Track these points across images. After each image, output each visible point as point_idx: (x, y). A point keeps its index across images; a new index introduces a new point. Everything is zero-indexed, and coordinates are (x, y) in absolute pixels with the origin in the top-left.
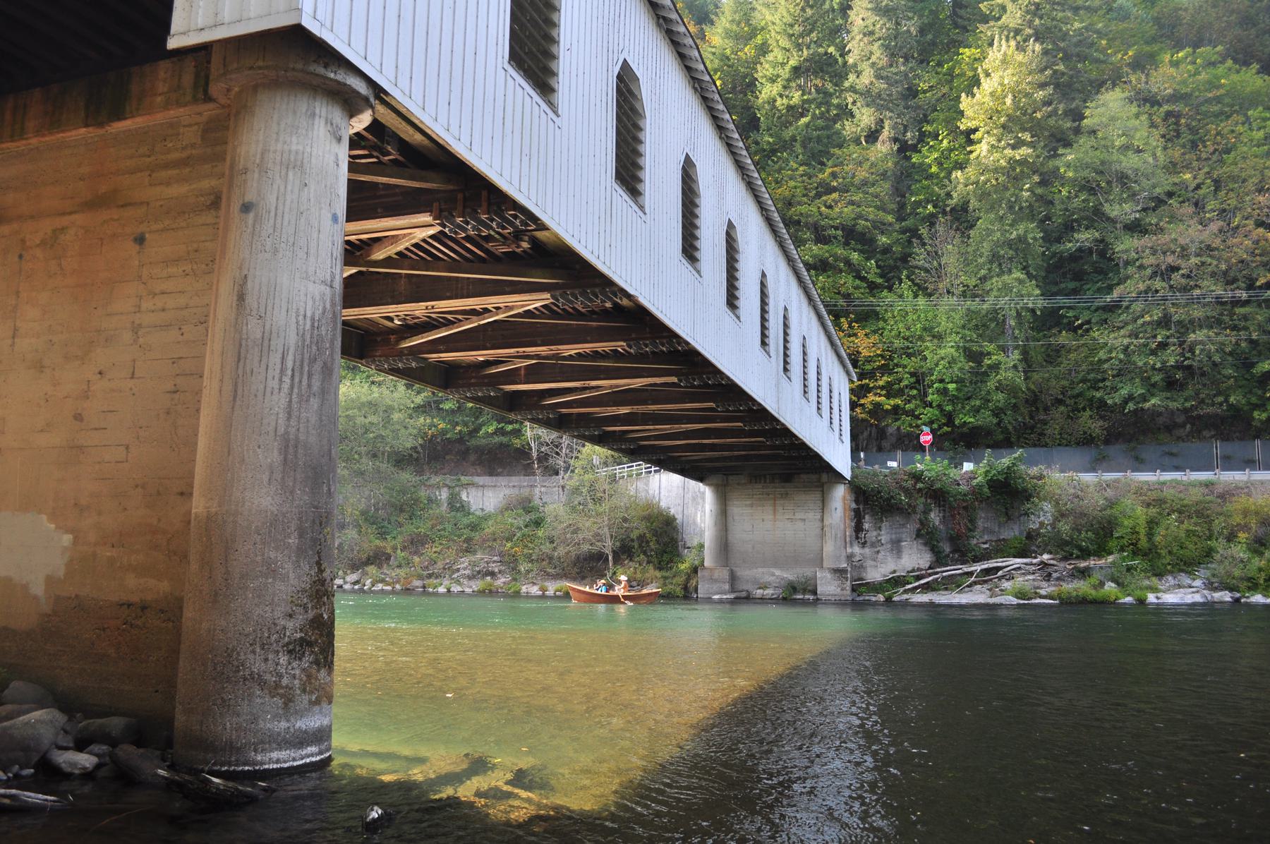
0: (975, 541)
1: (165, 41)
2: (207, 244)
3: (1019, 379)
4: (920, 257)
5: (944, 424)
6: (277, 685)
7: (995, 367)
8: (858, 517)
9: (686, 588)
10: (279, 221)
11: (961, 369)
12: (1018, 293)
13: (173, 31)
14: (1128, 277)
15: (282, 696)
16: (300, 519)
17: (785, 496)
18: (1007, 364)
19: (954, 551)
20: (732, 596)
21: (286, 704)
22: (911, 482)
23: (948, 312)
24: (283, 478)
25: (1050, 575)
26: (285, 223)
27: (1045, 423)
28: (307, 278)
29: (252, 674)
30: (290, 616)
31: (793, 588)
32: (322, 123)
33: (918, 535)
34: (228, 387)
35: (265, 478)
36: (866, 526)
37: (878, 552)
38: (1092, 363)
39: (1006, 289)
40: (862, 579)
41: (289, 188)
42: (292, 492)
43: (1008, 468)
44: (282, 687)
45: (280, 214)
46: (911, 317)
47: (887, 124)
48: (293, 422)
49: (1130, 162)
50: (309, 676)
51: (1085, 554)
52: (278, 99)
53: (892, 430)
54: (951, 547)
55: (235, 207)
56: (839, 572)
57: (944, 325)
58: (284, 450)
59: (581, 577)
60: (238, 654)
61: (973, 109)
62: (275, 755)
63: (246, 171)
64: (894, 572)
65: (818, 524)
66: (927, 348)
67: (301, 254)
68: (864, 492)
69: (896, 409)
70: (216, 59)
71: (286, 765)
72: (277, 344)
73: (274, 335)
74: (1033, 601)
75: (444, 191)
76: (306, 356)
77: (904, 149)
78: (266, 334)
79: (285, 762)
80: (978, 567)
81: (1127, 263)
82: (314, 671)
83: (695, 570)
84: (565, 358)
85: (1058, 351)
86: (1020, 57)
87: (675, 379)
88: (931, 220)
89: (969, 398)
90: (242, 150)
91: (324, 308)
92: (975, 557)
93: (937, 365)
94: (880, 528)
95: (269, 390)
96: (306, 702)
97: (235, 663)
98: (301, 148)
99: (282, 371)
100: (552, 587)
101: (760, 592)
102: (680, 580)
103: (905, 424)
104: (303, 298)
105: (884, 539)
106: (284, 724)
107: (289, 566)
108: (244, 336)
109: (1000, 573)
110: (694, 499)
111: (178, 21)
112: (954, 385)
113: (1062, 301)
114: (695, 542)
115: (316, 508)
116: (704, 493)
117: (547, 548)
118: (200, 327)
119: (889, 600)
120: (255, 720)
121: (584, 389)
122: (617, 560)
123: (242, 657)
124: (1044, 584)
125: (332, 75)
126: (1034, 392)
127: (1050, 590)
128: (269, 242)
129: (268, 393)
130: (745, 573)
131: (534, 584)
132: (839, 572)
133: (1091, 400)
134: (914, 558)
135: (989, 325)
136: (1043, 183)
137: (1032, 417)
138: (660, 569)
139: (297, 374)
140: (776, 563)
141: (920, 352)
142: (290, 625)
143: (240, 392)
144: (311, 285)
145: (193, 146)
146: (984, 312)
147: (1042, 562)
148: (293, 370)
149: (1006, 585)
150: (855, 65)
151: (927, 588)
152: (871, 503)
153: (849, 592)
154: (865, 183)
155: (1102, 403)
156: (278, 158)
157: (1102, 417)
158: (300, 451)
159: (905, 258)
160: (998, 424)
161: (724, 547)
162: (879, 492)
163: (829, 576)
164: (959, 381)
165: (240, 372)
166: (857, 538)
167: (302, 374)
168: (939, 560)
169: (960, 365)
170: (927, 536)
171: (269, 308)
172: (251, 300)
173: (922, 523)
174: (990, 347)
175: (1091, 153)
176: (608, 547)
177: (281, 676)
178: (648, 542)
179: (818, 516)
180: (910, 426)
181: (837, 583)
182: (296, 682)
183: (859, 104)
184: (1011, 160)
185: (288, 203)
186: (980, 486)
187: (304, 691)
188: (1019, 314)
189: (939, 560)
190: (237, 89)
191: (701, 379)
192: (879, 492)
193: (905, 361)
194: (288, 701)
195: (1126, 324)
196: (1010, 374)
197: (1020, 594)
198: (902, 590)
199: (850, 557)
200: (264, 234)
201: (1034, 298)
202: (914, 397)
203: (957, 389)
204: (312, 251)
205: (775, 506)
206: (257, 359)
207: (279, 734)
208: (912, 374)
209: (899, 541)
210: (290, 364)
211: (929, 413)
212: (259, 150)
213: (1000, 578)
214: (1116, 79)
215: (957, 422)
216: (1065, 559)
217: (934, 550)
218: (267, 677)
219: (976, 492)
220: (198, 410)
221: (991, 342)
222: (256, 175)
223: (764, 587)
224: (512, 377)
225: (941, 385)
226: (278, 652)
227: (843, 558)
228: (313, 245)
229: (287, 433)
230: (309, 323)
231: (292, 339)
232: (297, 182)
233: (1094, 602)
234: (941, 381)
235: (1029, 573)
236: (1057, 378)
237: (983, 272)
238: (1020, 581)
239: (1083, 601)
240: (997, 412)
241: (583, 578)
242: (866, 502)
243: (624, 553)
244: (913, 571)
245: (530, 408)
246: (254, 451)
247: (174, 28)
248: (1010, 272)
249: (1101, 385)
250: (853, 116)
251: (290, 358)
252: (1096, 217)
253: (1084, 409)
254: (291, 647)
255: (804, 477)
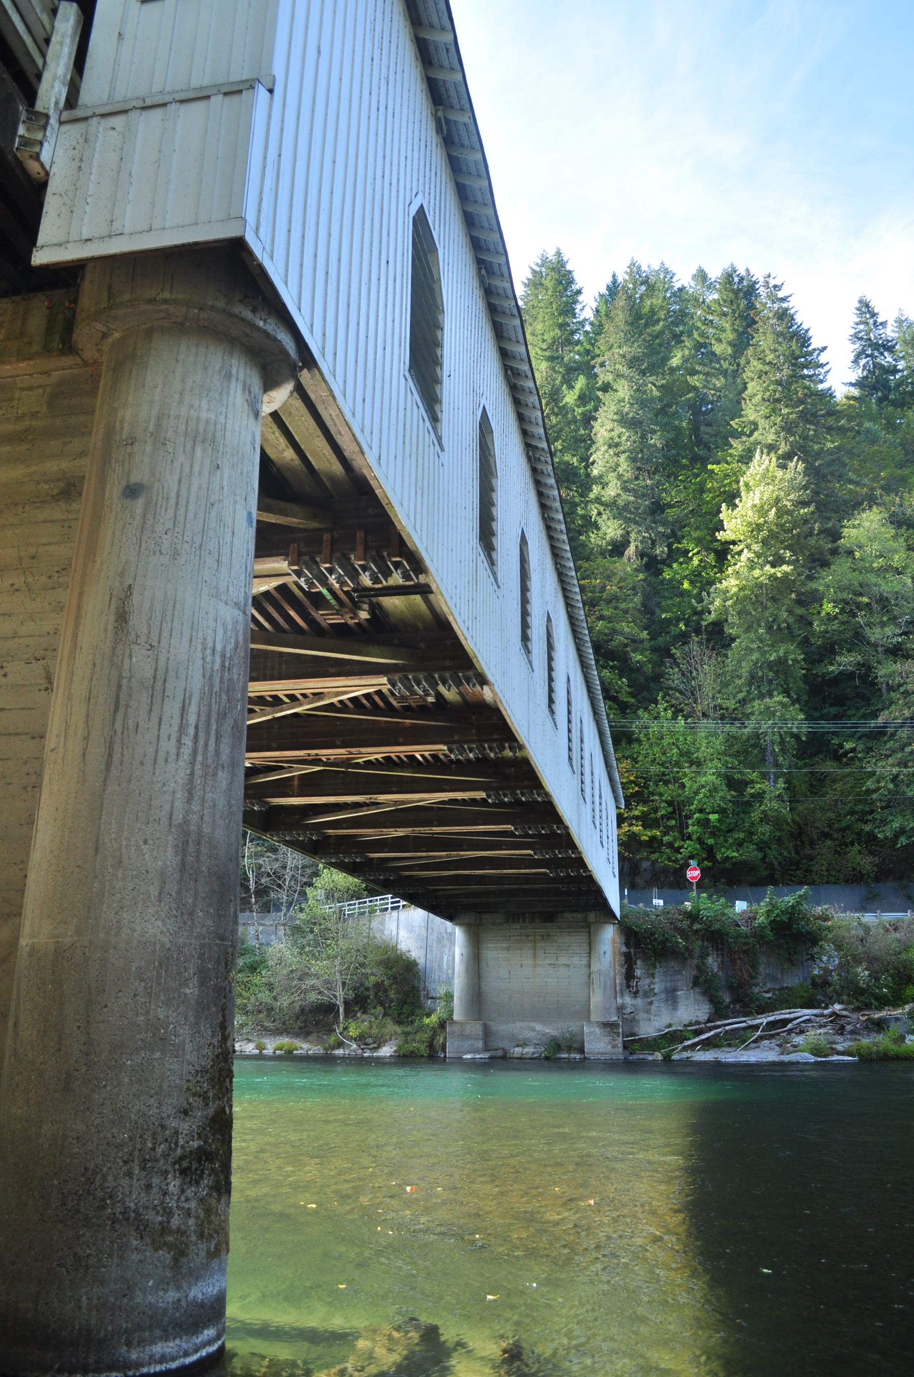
0: (756, 990)
1: (31, 253)
2: (51, 548)
3: (785, 811)
4: (674, 677)
5: (706, 859)
6: (165, 1229)
7: (759, 796)
8: (629, 962)
9: (431, 1046)
10: (182, 510)
11: (722, 798)
12: (778, 717)
13: (41, 240)
14: (892, 702)
15: (170, 1247)
16: (201, 956)
17: (547, 937)
18: (771, 793)
19: (734, 1001)
20: (486, 1055)
21: (176, 1260)
22: (686, 923)
23: (708, 738)
24: (179, 892)
25: (842, 1028)
26: (191, 515)
27: (811, 858)
28: (217, 596)
29: (126, 1210)
30: (186, 1112)
31: (556, 1045)
32: (240, 388)
33: (696, 983)
34: (97, 751)
35: (154, 891)
36: (638, 973)
37: (651, 1003)
38: (859, 794)
39: (769, 713)
40: (634, 1035)
41: (196, 468)
42: (191, 914)
43: (793, 907)
44: (171, 1232)
45: (183, 502)
46: (665, 742)
47: (633, 536)
48: (195, 807)
49: (889, 586)
50: (208, 1211)
51: (883, 1002)
52: (183, 348)
53: (645, 865)
54: (733, 997)
55: (114, 491)
56: (609, 1026)
57: (703, 751)
58: (182, 850)
59: (304, 1033)
60: (105, 1178)
61: (734, 523)
62: (158, 1349)
63: (132, 441)
64: (670, 1026)
65: (585, 971)
66: (685, 775)
67: (211, 561)
68: (636, 933)
69: (653, 839)
70: (90, 293)
71: (174, 1365)
72: (175, 687)
73: (171, 674)
74: (830, 1058)
75: (305, 530)
76: (215, 708)
77: (652, 564)
78: (160, 672)
79: (173, 1359)
80: (764, 1020)
81: (890, 688)
82: (213, 1202)
83: (442, 1025)
84: (358, 766)
85: (821, 781)
86: (780, 473)
87: (483, 795)
88: (684, 638)
89: (730, 831)
90: (127, 414)
91: (237, 642)
92: (759, 1007)
93: (696, 793)
94: (653, 976)
95: (161, 755)
96: (203, 1254)
97: (99, 1194)
98: (213, 416)
99: (182, 729)
100: (271, 1045)
101: (518, 1050)
102: (426, 1036)
103: (662, 859)
104: (211, 623)
105: (657, 988)
106: (172, 1295)
107: (185, 1032)
108: (126, 674)
109: (790, 1026)
110: (439, 940)
111: (48, 231)
112: (716, 816)
113: (826, 726)
114: (441, 991)
115: (222, 939)
116: (452, 934)
117: (265, 996)
118: (37, 667)
119: (667, 1058)
120: (129, 1289)
121: (357, 806)
122: (349, 1012)
123: (110, 1183)
124: (839, 1038)
125: (261, 324)
126: (798, 824)
127: (847, 1044)
128: (166, 541)
129: (161, 761)
130: (501, 1028)
131: (249, 1041)
132: (609, 1026)
133: (859, 834)
134: (691, 1010)
135: (750, 751)
136: (799, 602)
137: (797, 852)
138: (400, 1023)
139: (201, 735)
140: (537, 1015)
141: (676, 780)
142: (185, 1127)
143: (116, 757)
144: (221, 606)
145: (34, 415)
146: (744, 737)
147: (834, 1013)
148: (196, 727)
149: (798, 1040)
150: (601, 476)
151: (708, 1044)
152: (644, 947)
153: (620, 1050)
154: (614, 598)
155: (872, 837)
156: (182, 427)
157: (871, 852)
158: (204, 851)
159: (657, 678)
160: (763, 859)
161: (477, 996)
162: (653, 934)
163: (598, 1030)
164: (722, 811)
165: (118, 725)
166: (628, 986)
167: (208, 733)
168: (719, 1012)
169: (721, 794)
170: (703, 984)
171: (165, 634)
172: (138, 623)
173: (698, 967)
174: (754, 776)
175: (850, 576)
176: (340, 996)
177: (169, 1213)
178: (385, 991)
179: (584, 961)
180: (669, 859)
181: (607, 1039)
182: (192, 1221)
183: (604, 517)
184: (773, 578)
185: (194, 488)
186: (762, 927)
187: (201, 1236)
188: (782, 742)
189: (719, 1012)
190: (117, 335)
191: (514, 794)
192: (653, 934)
193: (662, 788)
194: (180, 1253)
195: (894, 752)
196: (775, 805)
197: (816, 1051)
198: (680, 1047)
199: (620, 1009)
200: (159, 528)
201: (797, 722)
202: (671, 828)
203: (719, 820)
204: (225, 559)
205: (535, 948)
206: (145, 708)
207: (165, 1311)
208: (670, 803)
209: (675, 990)
210: (192, 719)
211: (689, 847)
212: (155, 412)
213: (790, 1032)
214: (872, 501)
215: (719, 857)
216: (858, 1009)
217: (714, 1001)
218: (150, 1216)
219: (758, 934)
220: (37, 786)
221: (753, 768)
222: (149, 448)
223: (523, 1045)
224: (283, 787)
225: (702, 816)
226: (166, 1172)
227: (613, 1010)
228: (226, 551)
229: (186, 822)
230: (218, 660)
231: (197, 683)
232: (207, 462)
233: (898, 1058)
234: (701, 811)
235: (821, 1027)
236: (822, 809)
237: (740, 696)
238: (815, 1035)
239: (885, 1058)
240: (762, 846)
241: (308, 1034)
242: (637, 945)
243: (357, 1003)
244: (690, 1024)
245: (289, 828)
246: (138, 848)
247: (42, 239)
248: (771, 696)
249: (870, 817)
250: (598, 529)
251: (193, 709)
252: (857, 640)
253: (852, 844)
254: (185, 1164)
255: (568, 916)
